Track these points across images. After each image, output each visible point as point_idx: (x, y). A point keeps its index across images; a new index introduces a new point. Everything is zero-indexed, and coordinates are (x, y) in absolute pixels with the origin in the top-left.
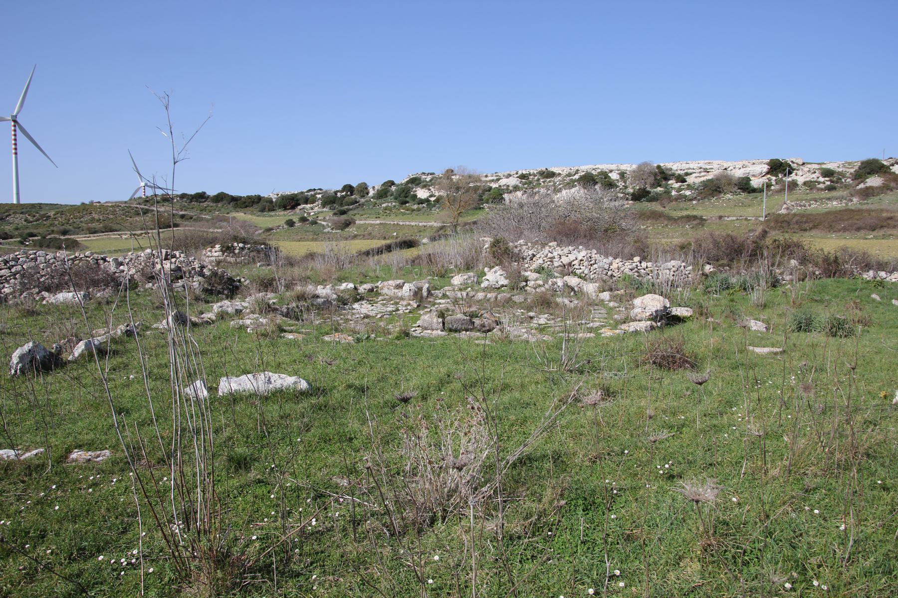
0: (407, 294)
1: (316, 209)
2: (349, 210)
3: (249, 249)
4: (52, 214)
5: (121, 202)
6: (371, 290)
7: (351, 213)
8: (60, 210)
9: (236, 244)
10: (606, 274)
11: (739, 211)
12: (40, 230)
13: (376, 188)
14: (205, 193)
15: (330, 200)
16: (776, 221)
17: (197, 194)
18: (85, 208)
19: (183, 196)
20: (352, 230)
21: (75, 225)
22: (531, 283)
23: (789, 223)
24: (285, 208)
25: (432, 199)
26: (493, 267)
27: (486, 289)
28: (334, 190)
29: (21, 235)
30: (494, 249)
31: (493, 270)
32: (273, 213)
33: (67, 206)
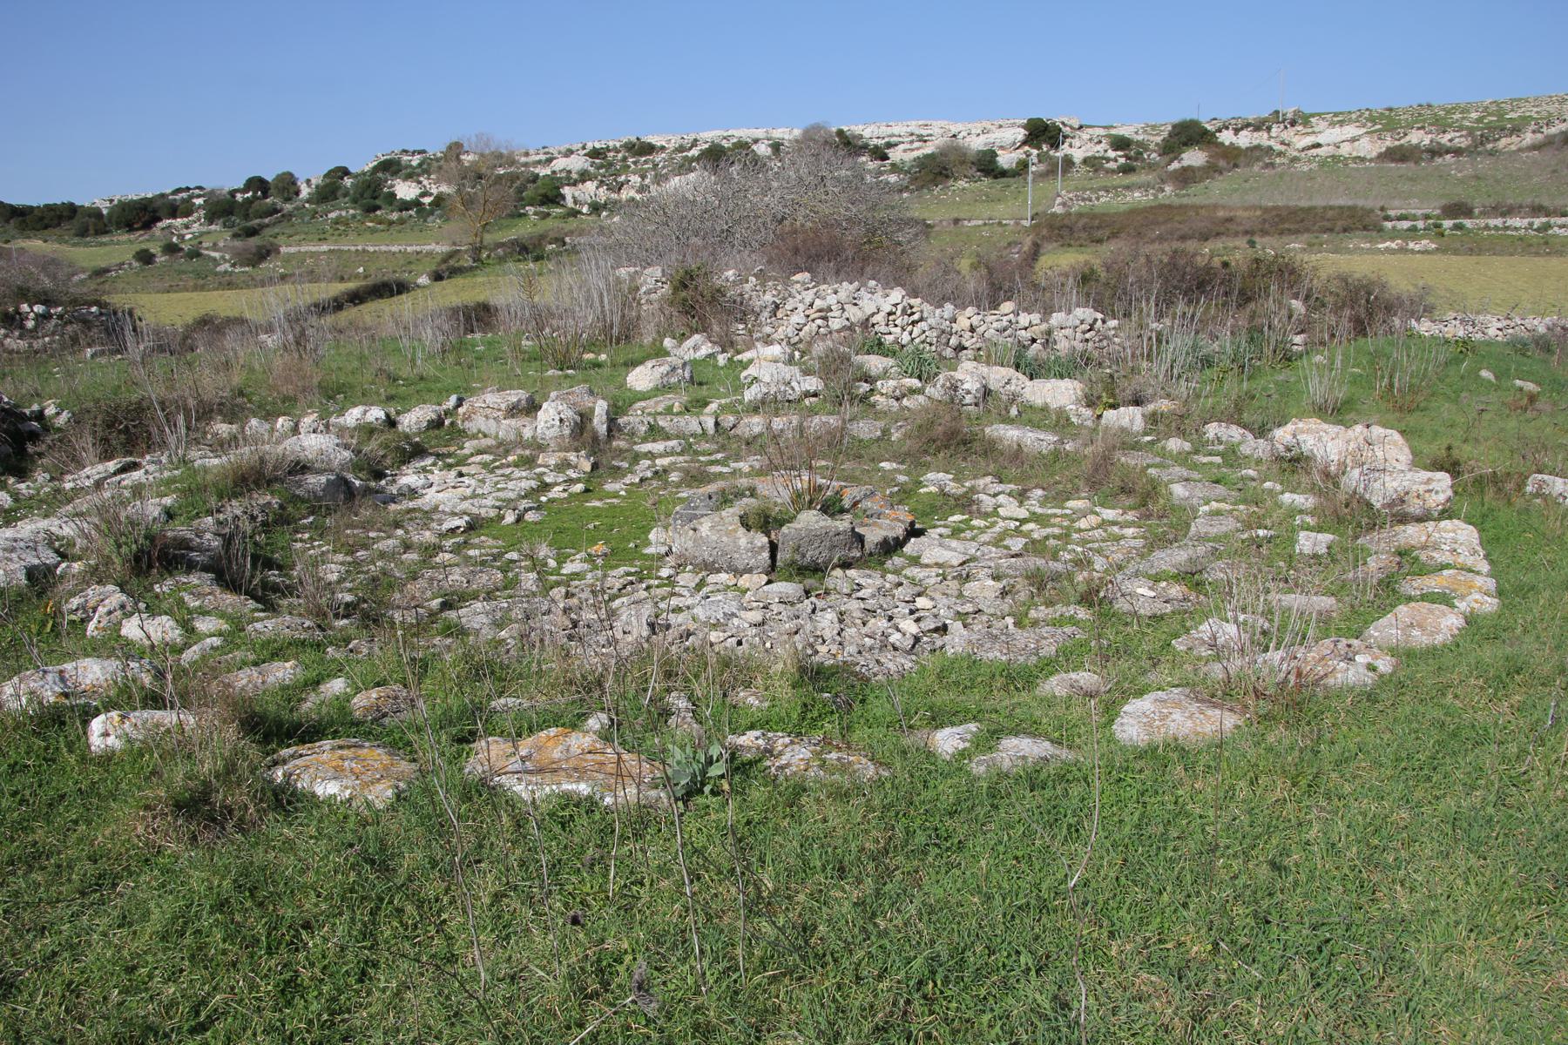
1: (196, 227)
2: (263, 227)
3: (60, 317)
7: (267, 232)
9: (25, 307)
11: (985, 210)
13: (314, 182)
15: (222, 208)
16: (1051, 227)
24: (130, 227)
25: (427, 200)
27: (755, 409)
28: (227, 188)
31: (689, 343)
32: (105, 239)
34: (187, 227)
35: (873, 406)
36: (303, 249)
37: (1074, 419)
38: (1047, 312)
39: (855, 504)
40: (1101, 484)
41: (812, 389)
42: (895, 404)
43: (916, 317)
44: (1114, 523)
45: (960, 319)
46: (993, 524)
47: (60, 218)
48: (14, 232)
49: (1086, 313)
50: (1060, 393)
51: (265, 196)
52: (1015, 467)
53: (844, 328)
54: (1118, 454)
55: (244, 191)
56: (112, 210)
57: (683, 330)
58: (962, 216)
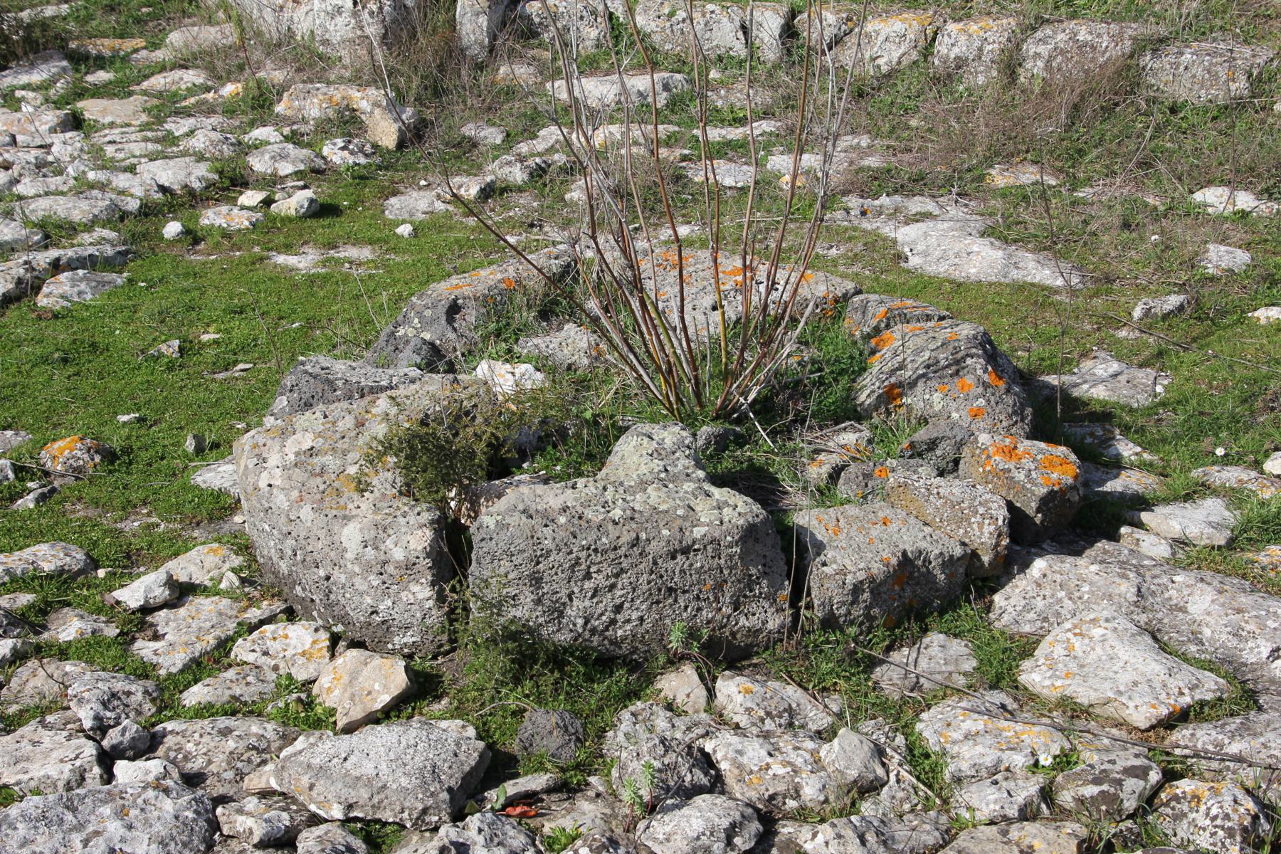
0: (340, 29)
39: (891, 395)
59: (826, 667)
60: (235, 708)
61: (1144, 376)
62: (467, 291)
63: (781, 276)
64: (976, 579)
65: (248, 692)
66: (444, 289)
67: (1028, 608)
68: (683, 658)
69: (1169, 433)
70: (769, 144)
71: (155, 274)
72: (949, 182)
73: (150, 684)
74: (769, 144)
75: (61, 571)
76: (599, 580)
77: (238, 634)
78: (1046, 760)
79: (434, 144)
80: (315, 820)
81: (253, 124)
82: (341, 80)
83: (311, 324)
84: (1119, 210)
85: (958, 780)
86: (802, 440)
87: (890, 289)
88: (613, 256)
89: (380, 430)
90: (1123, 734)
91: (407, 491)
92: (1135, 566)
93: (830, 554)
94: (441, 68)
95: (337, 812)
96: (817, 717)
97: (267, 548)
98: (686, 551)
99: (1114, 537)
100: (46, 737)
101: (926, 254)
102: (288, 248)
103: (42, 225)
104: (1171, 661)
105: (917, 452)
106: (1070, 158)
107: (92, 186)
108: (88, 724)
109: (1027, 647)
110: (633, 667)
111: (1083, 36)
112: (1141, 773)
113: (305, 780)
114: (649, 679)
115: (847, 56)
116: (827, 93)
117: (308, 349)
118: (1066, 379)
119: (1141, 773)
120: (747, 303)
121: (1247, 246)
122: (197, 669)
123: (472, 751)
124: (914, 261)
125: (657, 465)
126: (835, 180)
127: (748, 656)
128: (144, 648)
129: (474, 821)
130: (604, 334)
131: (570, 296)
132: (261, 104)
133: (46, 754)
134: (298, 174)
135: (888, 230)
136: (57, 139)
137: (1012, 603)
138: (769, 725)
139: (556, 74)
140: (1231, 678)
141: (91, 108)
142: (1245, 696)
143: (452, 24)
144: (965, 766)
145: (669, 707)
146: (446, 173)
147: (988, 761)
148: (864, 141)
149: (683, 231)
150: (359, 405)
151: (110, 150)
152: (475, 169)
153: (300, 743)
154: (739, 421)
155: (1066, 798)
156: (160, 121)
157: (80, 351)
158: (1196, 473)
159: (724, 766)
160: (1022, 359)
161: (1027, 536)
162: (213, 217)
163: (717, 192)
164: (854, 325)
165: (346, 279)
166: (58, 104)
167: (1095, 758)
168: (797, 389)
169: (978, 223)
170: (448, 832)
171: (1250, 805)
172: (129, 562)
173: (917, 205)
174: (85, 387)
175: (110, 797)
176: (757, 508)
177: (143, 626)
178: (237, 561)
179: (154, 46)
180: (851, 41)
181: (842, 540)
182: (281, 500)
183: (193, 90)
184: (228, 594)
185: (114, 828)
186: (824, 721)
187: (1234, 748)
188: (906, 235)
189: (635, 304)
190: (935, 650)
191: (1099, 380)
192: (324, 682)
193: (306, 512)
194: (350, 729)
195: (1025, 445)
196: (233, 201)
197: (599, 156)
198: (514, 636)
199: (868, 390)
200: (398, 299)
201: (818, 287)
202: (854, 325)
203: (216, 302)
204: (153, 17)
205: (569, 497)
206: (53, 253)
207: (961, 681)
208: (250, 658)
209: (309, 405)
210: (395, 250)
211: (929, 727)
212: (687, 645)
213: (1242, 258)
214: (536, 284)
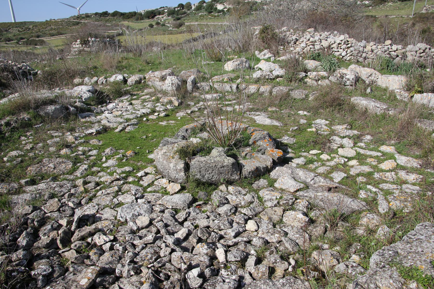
0: (170, 88)
2: (181, 17)
3: (99, 41)
4: (31, 27)
5: (65, 19)
6: (139, 82)
7: (182, 19)
8: (35, 24)
9: (90, 39)
10: (361, 56)
11: (397, 13)
12: (26, 36)
13: (196, 5)
14: (107, 12)
15: (172, 12)
16: (420, 18)
17: (103, 12)
18: (47, 23)
19: (96, 14)
20: (183, 28)
21: (43, 32)
22: (312, 75)
23: (428, 18)
24: (149, 18)
25: (225, 10)
26: (263, 50)
27: (257, 81)
28: (174, 6)
29: (16, 39)
30: (263, 35)
31: (263, 53)
32: (142, 21)
33: (38, 22)
34: (163, 18)
35: (306, 83)
36: (191, 23)
37: (398, 97)
38: (405, 45)
39: (254, 143)
40: (404, 137)
41: (280, 74)
42: (315, 83)
43: (349, 45)
44: (403, 168)
45: (367, 47)
46: (332, 159)
47: (132, 15)
48: (121, 19)
49: (423, 46)
50: (394, 83)
51: (183, 9)
52: (360, 120)
53: (321, 49)
54: (416, 121)
55: (178, 8)
56: (145, 13)
57: (262, 48)
58: (389, 14)
59: (245, 184)
60: (155, 191)
61: (292, 139)
62: (189, 127)
63: (237, 124)
64: (268, 170)
65: (157, 189)
66: (185, 127)
67: (275, 175)
68: (223, 183)
69: (296, 148)
70: (235, 104)
71: (142, 126)
72: (262, 110)
73: (142, 188)
74: (235, 104)
75: (129, 171)
76: (210, 172)
77: (155, 180)
78: (278, 198)
79: (184, 105)
80: (167, 208)
81: (156, 103)
82: (170, 96)
83: (165, 133)
84: (288, 114)
85: (265, 201)
86: (241, 149)
87: (254, 126)
88: (211, 121)
89: (176, 149)
90: (289, 193)
91: (180, 158)
92: (291, 168)
93: (245, 167)
94: (185, 94)
95: (171, 207)
96: (244, 192)
97: (159, 167)
98: (223, 167)
99: (288, 164)
100: (128, 195)
101: (259, 121)
102: (162, 121)
103: (126, 119)
104: (296, 182)
105: (259, 151)
106: (280, 106)
107: (133, 113)
108: (134, 194)
109: (275, 181)
110: (215, 185)
111: (281, 88)
112: (292, 199)
113: (166, 202)
114: (218, 187)
115: (246, 91)
116: (244, 97)
117: (165, 137)
118: (281, 140)
119: (292, 199)
120: (232, 128)
121: (306, 120)
122: (149, 186)
123: (191, 198)
124: (257, 122)
125: (219, 154)
126: (245, 110)
127: (233, 183)
128: (141, 182)
129: (191, 209)
130: (210, 134)
131: (205, 128)
132: (158, 100)
133: (128, 198)
134: (163, 110)
135: (253, 117)
136: (128, 107)
137: (273, 174)
138: (236, 193)
139: (202, 94)
140: (305, 184)
141: (133, 102)
142: (307, 187)
143: (186, 87)
144: (266, 199)
145: (221, 191)
146: (185, 110)
147: (270, 198)
148: (249, 104)
149: (222, 117)
150: (172, 145)
151: (136, 108)
152: (190, 109)
153: (165, 197)
154: (231, 147)
155: (281, 203)
156: (143, 103)
157: (132, 138)
158: (300, 154)
159: (229, 200)
160: (274, 137)
161: (275, 164)
162: (151, 117)
163: (227, 112)
164: (249, 132)
165: (170, 126)
166: (129, 101)
167: (285, 197)
168: (240, 141)
169: (267, 116)
170: (187, 210)
171: (307, 203)
172: (139, 170)
173: (257, 113)
174: (132, 143)
175: (137, 205)
176: (234, 160)
177: (141, 179)
178: (155, 169)
179: (143, 92)
180: (247, 89)
181: (247, 165)
182: (161, 160)
183: (148, 98)
184: (153, 174)
185: (138, 209)
186: (245, 193)
187: (305, 195)
188: (256, 118)
189: (215, 129)
190: (262, 181)
191: (285, 140)
192: (168, 187)
193: (165, 162)
194: (172, 195)
195: (275, 150)
196: (153, 115)
197: (209, 106)
198: (197, 180)
199: (251, 142)
200: (178, 129)
201: (243, 126)
202: (249, 132)
203: (151, 130)
204: (142, 88)
205: (205, 159)
206: (128, 123)
207: (266, 186)
208: (157, 184)
209: (165, 145)
210: (178, 121)
211: (261, 193)
212: (223, 181)
213: (305, 121)
214: (199, 126)
